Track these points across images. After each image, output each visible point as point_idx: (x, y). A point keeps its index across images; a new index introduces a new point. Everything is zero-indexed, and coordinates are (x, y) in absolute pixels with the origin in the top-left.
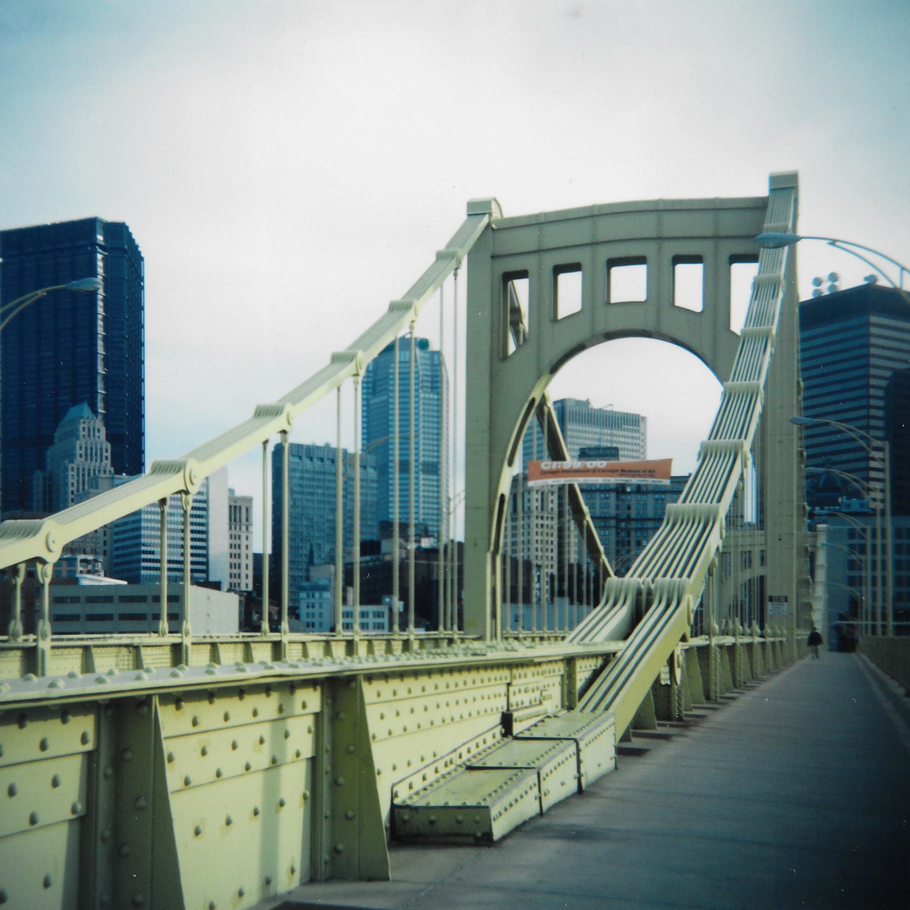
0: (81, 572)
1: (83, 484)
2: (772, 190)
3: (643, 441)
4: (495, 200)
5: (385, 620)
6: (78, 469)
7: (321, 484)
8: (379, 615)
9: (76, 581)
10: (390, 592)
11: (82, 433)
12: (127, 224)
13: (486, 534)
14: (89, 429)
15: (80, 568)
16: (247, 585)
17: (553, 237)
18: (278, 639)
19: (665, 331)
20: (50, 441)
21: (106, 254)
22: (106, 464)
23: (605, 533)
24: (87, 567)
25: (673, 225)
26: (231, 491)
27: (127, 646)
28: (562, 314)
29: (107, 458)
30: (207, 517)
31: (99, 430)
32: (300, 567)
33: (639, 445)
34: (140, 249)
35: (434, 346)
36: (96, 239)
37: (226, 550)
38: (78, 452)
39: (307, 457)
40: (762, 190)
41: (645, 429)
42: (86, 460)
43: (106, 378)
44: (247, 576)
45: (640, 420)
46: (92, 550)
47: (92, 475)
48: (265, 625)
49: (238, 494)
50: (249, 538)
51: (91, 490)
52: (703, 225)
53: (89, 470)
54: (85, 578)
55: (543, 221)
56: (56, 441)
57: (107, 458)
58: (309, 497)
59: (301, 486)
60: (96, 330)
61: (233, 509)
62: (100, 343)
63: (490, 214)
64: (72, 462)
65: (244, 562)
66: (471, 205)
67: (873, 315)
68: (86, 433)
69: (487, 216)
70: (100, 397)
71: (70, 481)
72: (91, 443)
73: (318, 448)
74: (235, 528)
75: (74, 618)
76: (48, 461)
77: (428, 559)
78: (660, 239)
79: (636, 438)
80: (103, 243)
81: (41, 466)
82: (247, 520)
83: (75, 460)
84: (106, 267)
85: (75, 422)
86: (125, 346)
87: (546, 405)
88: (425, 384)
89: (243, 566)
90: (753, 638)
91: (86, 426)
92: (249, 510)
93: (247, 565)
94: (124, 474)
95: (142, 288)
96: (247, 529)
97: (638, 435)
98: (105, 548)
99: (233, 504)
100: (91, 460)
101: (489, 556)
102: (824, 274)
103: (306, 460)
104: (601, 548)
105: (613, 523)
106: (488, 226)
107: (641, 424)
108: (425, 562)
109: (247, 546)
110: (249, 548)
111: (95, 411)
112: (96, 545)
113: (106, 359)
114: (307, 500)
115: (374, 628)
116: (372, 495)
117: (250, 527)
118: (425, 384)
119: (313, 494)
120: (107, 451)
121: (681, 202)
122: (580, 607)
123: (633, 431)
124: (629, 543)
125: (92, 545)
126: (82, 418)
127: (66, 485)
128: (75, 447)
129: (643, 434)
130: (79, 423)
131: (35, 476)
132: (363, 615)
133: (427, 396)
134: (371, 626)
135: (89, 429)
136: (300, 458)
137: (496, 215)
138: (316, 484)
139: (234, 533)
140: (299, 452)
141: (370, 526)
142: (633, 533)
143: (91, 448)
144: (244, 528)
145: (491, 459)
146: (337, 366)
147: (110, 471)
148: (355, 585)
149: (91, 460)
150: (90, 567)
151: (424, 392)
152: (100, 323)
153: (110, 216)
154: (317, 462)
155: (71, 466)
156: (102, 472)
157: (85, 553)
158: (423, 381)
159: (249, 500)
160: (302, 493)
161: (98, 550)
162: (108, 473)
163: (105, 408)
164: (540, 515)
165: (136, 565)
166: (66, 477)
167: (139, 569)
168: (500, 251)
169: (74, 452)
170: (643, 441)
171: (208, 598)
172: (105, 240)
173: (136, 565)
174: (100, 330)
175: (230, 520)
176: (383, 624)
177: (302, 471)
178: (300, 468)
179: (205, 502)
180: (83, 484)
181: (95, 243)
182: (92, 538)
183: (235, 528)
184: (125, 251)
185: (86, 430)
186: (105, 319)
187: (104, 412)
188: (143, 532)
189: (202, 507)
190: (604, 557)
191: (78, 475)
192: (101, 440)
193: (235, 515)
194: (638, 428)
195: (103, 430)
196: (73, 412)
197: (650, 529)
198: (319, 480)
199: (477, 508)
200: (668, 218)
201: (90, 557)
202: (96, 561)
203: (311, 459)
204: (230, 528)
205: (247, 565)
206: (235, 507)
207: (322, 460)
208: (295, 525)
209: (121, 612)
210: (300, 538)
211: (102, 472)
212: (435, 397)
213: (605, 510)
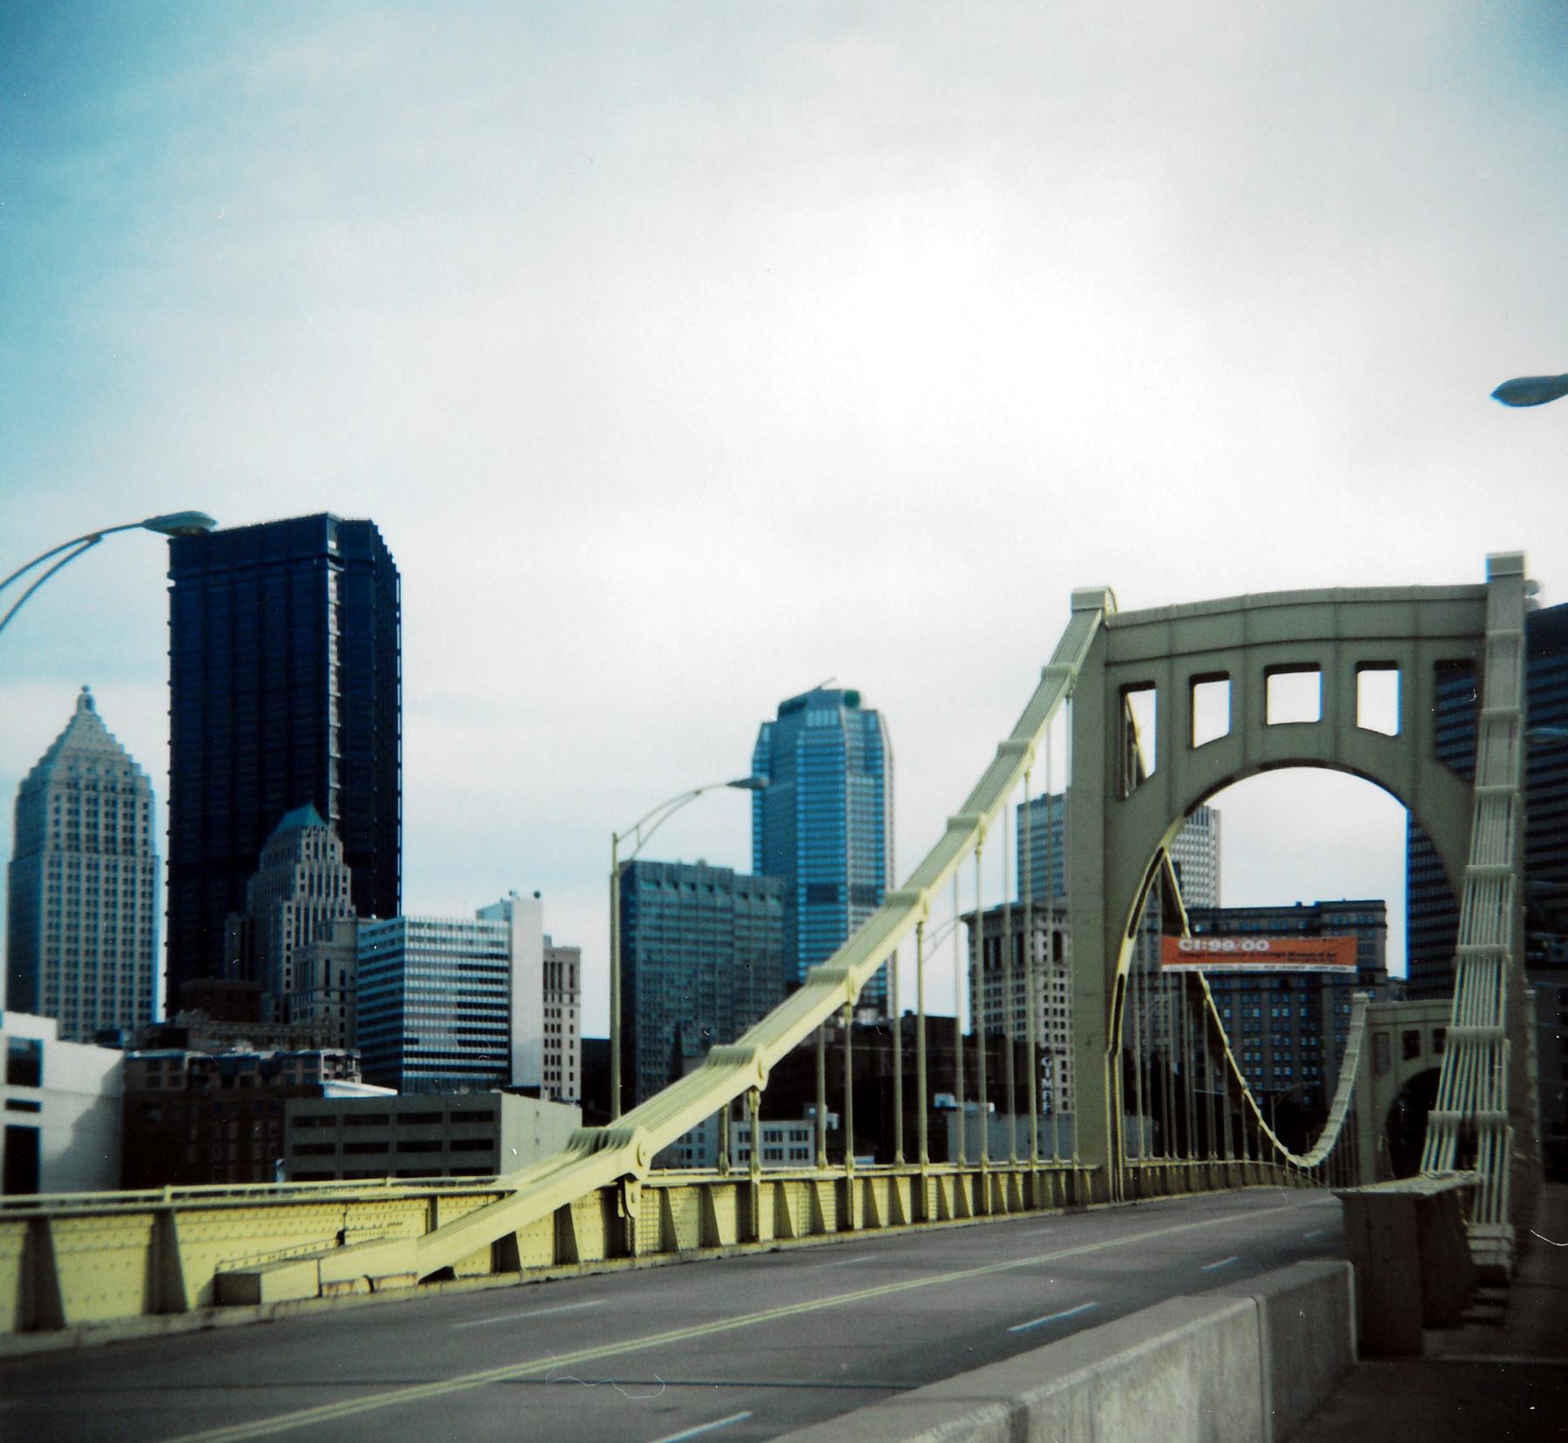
0: (326, 1076)
1: (306, 932)
2: (1491, 578)
3: (1214, 848)
4: (1110, 590)
5: (809, 1145)
6: (298, 909)
7: (692, 924)
8: (799, 1136)
9: (318, 1091)
10: (814, 1100)
11: (304, 852)
12: (375, 523)
13: (1103, 1030)
14: (316, 845)
15: (324, 1071)
16: (571, 1091)
17: (1188, 638)
18: (916, 1171)
19: (1347, 761)
20: (252, 865)
21: (342, 570)
22: (343, 901)
24: (334, 1068)
25: (1354, 622)
26: (548, 940)
27: (804, 1181)
29: (344, 891)
30: (509, 982)
31: (332, 847)
32: (659, 1059)
33: (1208, 854)
34: (394, 561)
35: (868, 702)
36: (326, 546)
37: (539, 1034)
38: (299, 882)
39: (669, 881)
40: (1477, 575)
41: (1218, 830)
42: (311, 893)
43: (341, 764)
44: (571, 1076)
45: (1210, 816)
46: (323, 1038)
47: (320, 918)
48: (900, 1156)
49: (557, 943)
50: (575, 1014)
51: (320, 943)
52: (1399, 622)
53: (315, 911)
54: (333, 1085)
55: (1175, 617)
56: (262, 865)
57: (344, 891)
58: (673, 947)
59: (660, 929)
60: (327, 690)
61: (549, 968)
62: (332, 709)
63: (1103, 609)
64: (288, 898)
65: (566, 1052)
66: (1077, 598)
68: (311, 852)
69: (1100, 612)
70: (332, 796)
71: (285, 929)
72: (320, 869)
73: (687, 868)
74: (553, 999)
75: (433, 1147)
76: (250, 897)
77: (871, 1043)
78: (1338, 640)
79: (1203, 844)
80: (336, 554)
81: (236, 902)
82: (572, 984)
83: (293, 895)
84: (340, 589)
85: (295, 833)
86: (372, 713)
88: (855, 762)
89: (565, 1061)
90: (921, 1168)
91: (312, 841)
92: (575, 969)
93: (571, 1059)
94: (374, 917)
95: (398, 621)
96: (572, 999)
97: (1207, 840)
98: (342, 1035)
99: (550, 960)
100: (319, 894)
101: (1106, 1056)
103: (667, 888)
104: (1225, 1038)
106: (1102, 624)
107: (1212, 822)
108: (867, 1048)
109: (572, 1029)
110: (575, 1030)
111: (324, 816)
112: (330, 1032)
113: (341, 735)
114: (669, 952)
115: (792, 1157)
116: (776, 941)
117: (576, 997)
118: (855, 762)
119: (678, 941)
120: (345, 879)
121: (1366, 591)
122: (1132, 1118)
123: (1198, 832)
125: (324, 1031)
126: (306, 828)
127: (278, 934)
128: (294, 876)
129: (1214, 838)
130: (300, 836)
131: (227, 923)
132: (772, 1136)
133: (858, 780)
134: (786, 1154)
135: (316, 845)
136: (658, 884)
137: (1109, 609)
138: (683, 924)
139: (550, 1007)
140: (654, 874)
141: (771, 991)
143: (320, 876)
144: (566, 998)
145: (1106, 930)
146: (956, 835)
147: (350, 911)
149: (319, 894)
150: (339, 1068)
151: (855, 775)
152: (332, 678)
153: (347, 509)
154: (684, 889)
155: (286, 904)
156: (337, 913)
157: (330, 1045)
158: (851, 758)
159: (575, 953)
160: (661, 940)
161: (332, 1039)
162: (346, 914)
163: (339, 812)
165: (394, 1062)
166: (278, 922)
167: (400, 1068)
168: (1118, 657)
169: (292, 882)
170: (1214, 848)
172: (339, 547)
173: (394, 1062)
174: (333, 690)
175: (545, 986)
176: (806, 1150)
177: (662, 905)
178: (658, 899)
179: (507, 957)
180: (306, 932)
181: (324, 555)
182: (324, 1020)
183: (553, 999)
184: (372, 565)
185: (312, 847)
186: (340, 672)
187: (338, 817)
188: (407, 1009)
189: (497, 965)
190: (1228, 1051)
191: (298, 919)
192: (336, 862)
193: (552, 975)
194: (1206, 829)
195: (339, 846)
196: (290, 820)
197: (1236, 990)
198: (688, 919)
199: (1088, 995)
200: (1349, 613)
201: (340, 1053)
202: (349, 1058)
203: (676, 886)
204: (545, 999)
205: (571, 1059)
206: (553, 964)
207: (693, 887)
208: (649, 992)
209: (402, 1138)
210: (659, 1012)
211: (337, 913)
212: (872, 782)
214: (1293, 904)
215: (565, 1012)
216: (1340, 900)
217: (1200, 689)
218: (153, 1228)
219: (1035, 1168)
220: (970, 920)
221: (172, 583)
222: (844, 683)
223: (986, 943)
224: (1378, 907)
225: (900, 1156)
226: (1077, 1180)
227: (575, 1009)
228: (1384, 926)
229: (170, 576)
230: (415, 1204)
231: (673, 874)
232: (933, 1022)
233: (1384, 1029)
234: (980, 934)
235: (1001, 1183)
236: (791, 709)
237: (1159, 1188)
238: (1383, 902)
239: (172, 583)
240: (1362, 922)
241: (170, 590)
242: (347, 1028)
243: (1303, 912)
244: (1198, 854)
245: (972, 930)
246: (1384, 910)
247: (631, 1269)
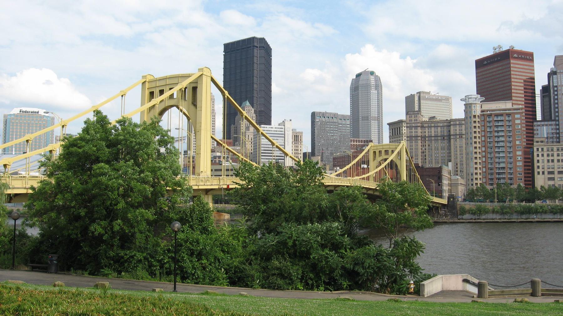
41: (451, 102)
95: (271, 59)
102: (496, 46)
105: (420, 138)
124: (425, 145)
142: (427, 142)
153: (259, 36)
213: (416, 134)
215: (299, 146)
216: (490, 53)
221: (224, 53)
222: (370, 69)
229: (224, 52)
231: (323, 115)
236: (358, 76)
239: (224, 53)
241: (224, 55)
242: (252, 150)
244: (504, 76)
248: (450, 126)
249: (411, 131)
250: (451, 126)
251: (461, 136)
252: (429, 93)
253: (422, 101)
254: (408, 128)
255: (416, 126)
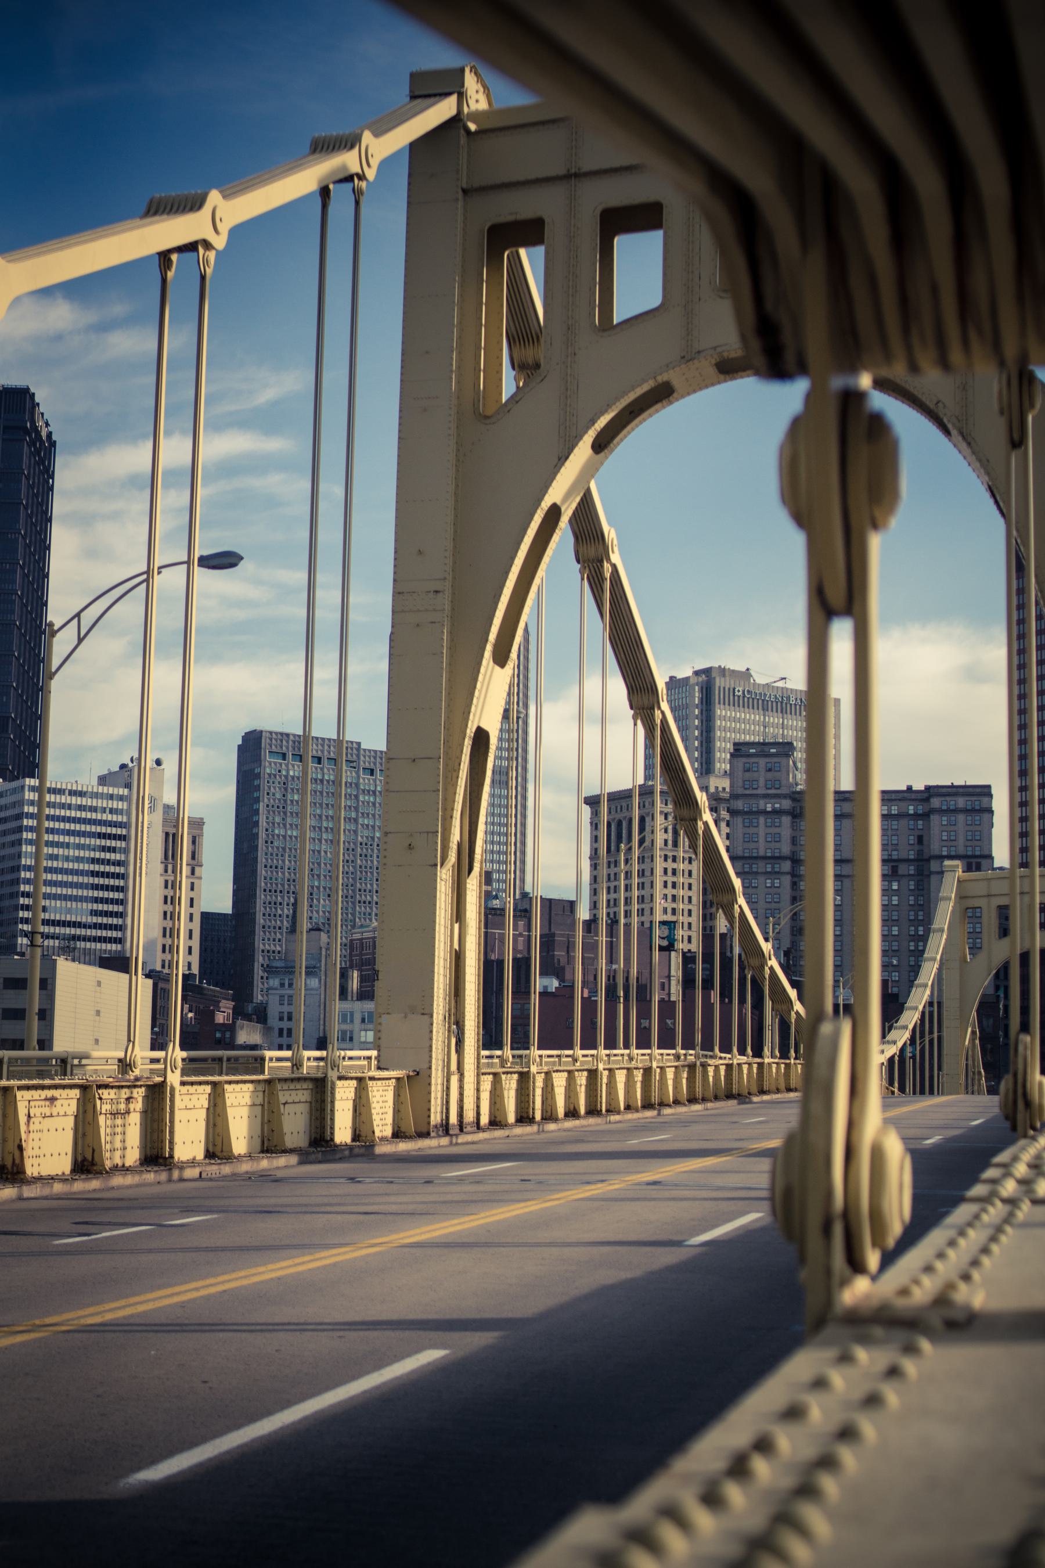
23: (773, 883)
28: (618, 316)
30: (126, 851)
48: (735, 1050)
67: (763, 1230)
69: (454, 98)
87: (609, 560)
101: (445, 877)
106: (455, 122)
117: (197, 869)
148: (1031, 1031)
164: (670, 854)
171: (99, 984)
184: (27, 432)
213: (773, 845)
214: (905, 788)
217: (621, 243)
218: (587, 1077)
219: (735, 1062)
220: (593, 802)
223: (609, 825)
224: (985, 791)
225: (735, 1050)
226: (735, 1073)
227: (196, 881)
228: (992, 812)
230: (201, 1089)
232: (549, 904)
233: (976, 903)
234: (605, 817)
235: (618, 1079)
237: (782, 1086)
238: (989, 787)
240: (969, 807)
243: (913, 796)
245: (595, 814)
246: (991, 796)
247: (20, 1198)
248: (926, 816)
249: (752, 830)
250: (932, 817)
251: (974, 860)
252: (747, 674)
253: (719, 711)
254: (739, 820)
255: (750, 813)
